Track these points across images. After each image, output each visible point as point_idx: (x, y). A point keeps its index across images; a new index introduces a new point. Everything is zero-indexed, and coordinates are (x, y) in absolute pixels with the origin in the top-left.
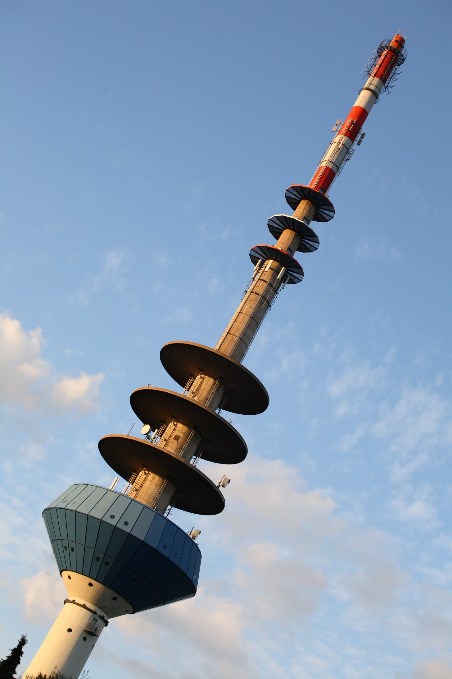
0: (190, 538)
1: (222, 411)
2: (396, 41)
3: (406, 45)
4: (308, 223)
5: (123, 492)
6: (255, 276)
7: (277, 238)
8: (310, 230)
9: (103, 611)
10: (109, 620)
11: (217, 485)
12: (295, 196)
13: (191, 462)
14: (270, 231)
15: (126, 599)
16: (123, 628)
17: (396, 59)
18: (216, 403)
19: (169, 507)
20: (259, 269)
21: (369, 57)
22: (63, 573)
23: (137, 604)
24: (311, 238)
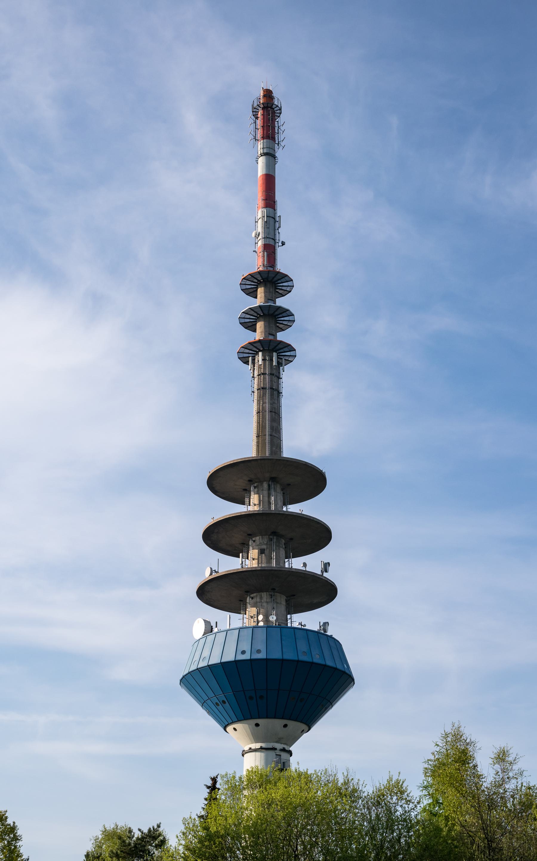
0: (322, 634)
1: (289, 506)
2: (264, 96)
3: (275, 94)
4: (275, 303)
5: (241, 626)
6: (254, 374)
7: (255, 331)
8: (279, 308)
9: (281, 743)
10: (290, 749)
11: (319, 573)
12: (251, 284)
13: (287, 566)
14: (245, 328)
15: (296, 720)
17: (274, 112)
18: (280, 503)
19: (289, 616)
20: (254, 366)
21: (249, 125)
22: (228, 729)
23: (308, 716)
24: (284, 314)
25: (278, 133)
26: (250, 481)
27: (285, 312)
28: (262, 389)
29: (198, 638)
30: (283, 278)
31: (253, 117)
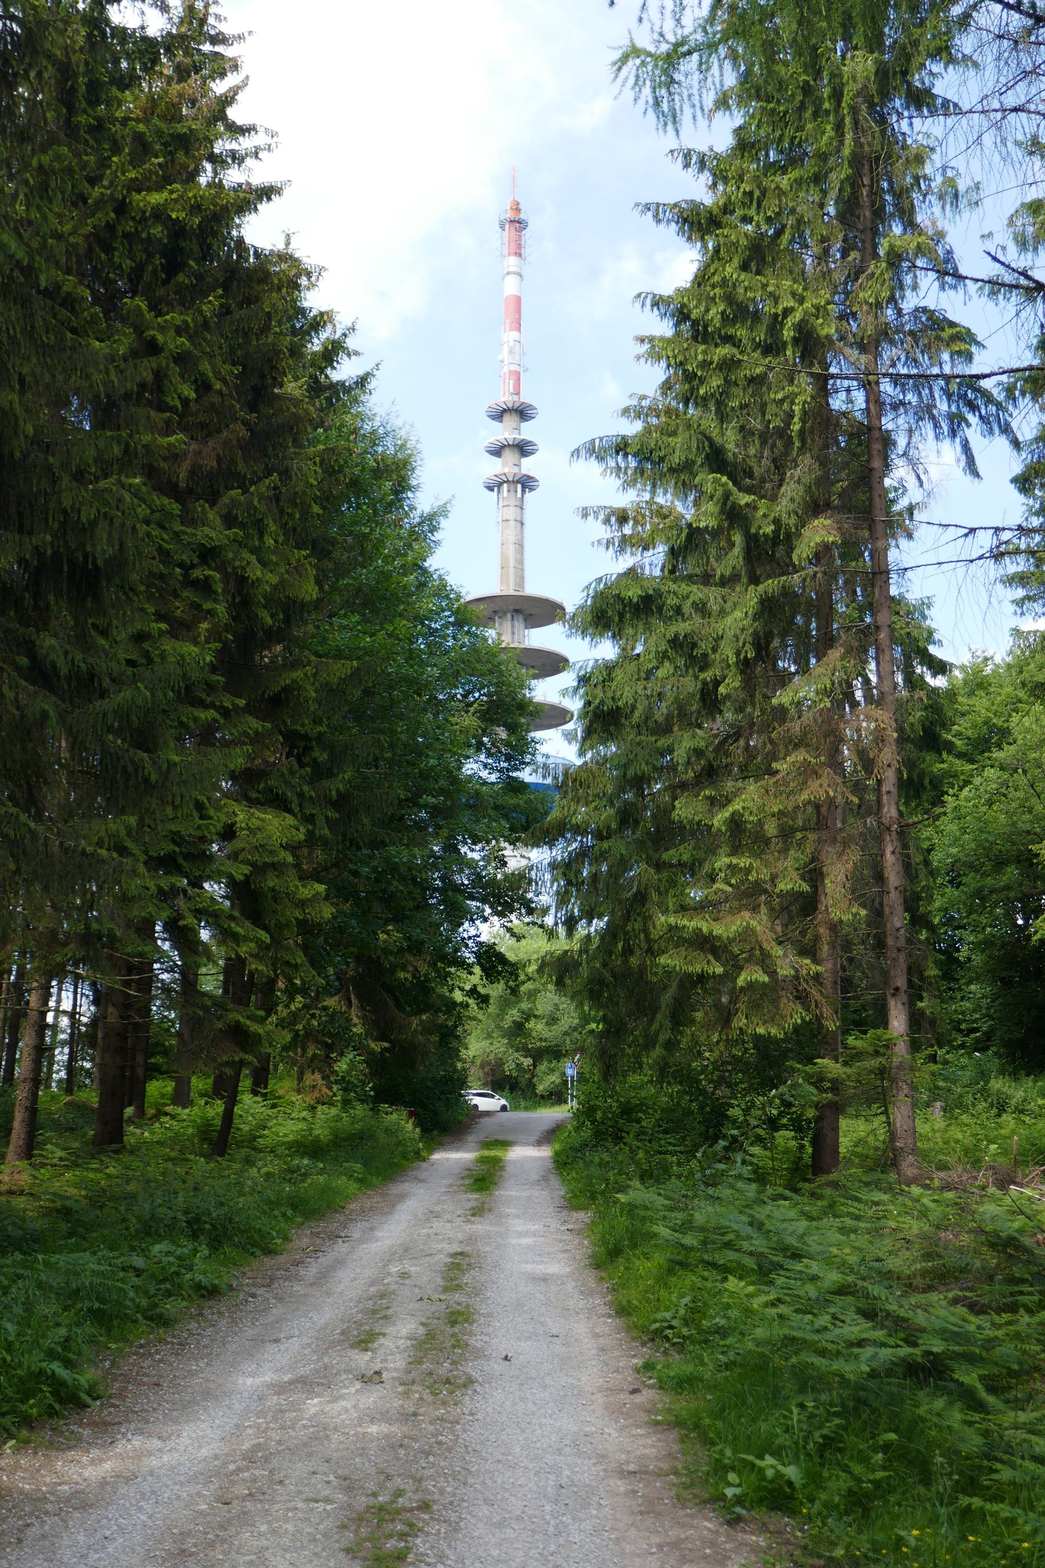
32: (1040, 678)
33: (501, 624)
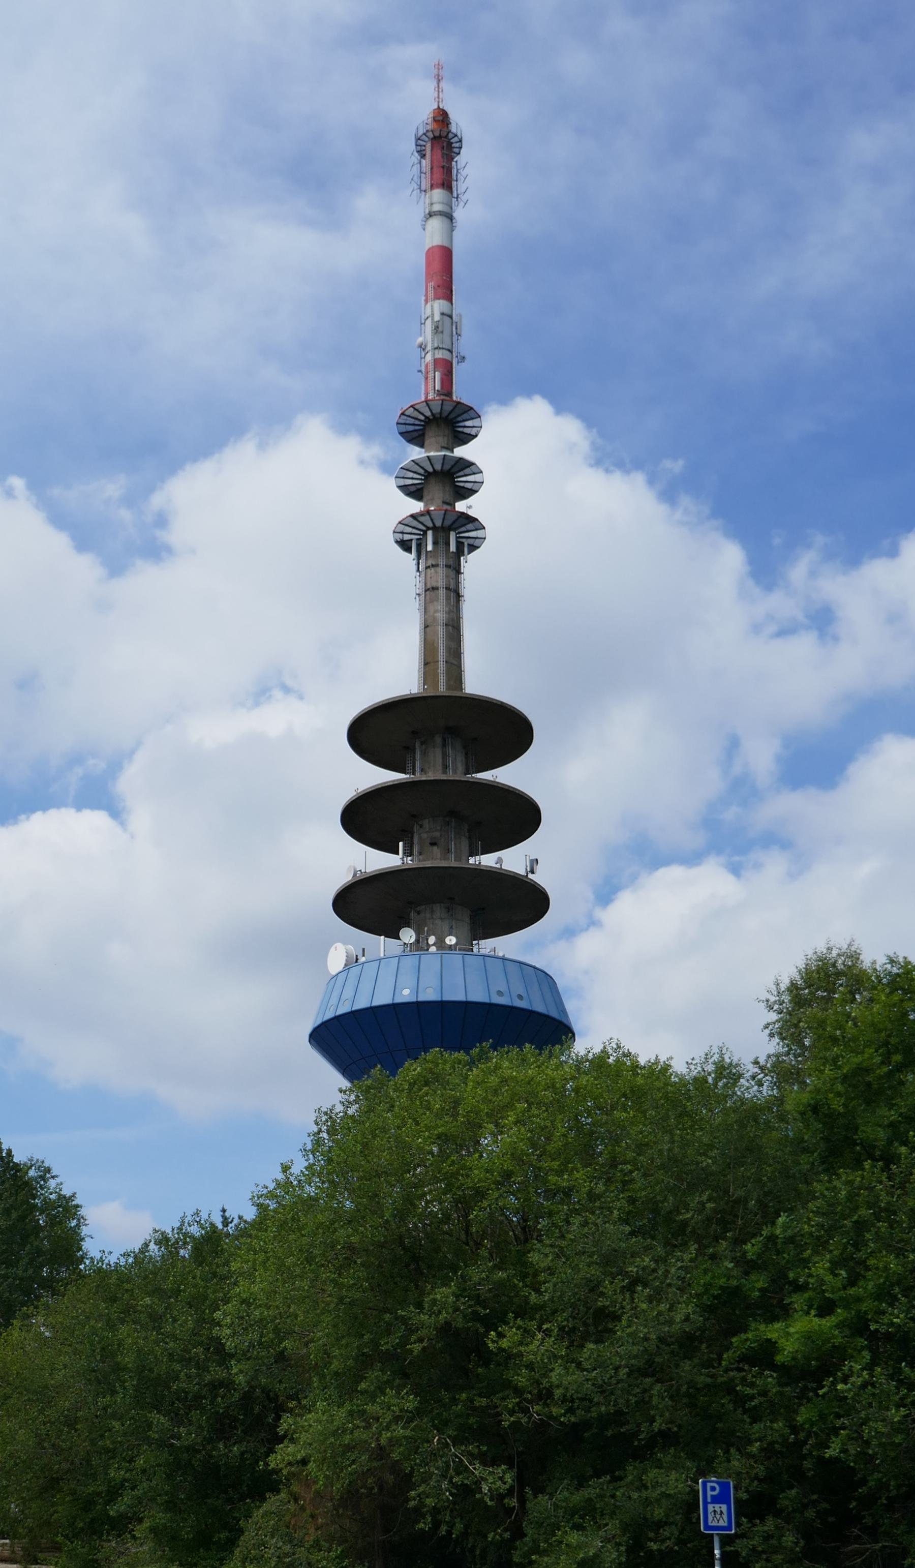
4: (453, 452)
11: (523, 873)
16: (436, 107)
17: (450, 144)
21: (411, 165)
25: (457, 198)
26: (413, 732)
27: (469, 466)
28: (430, 590)
29: (334, 973)
30: (465, 412)
31: (416, 154)
32: (870, 1413)
33: (424, 754)
